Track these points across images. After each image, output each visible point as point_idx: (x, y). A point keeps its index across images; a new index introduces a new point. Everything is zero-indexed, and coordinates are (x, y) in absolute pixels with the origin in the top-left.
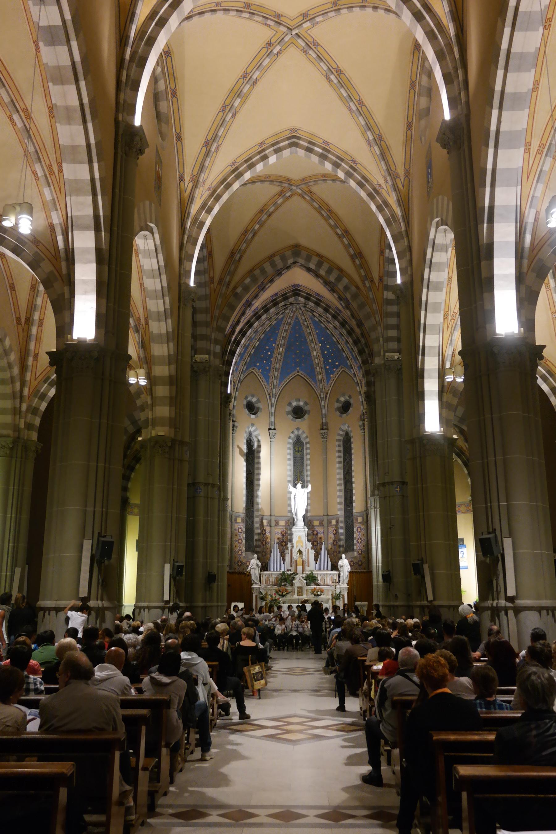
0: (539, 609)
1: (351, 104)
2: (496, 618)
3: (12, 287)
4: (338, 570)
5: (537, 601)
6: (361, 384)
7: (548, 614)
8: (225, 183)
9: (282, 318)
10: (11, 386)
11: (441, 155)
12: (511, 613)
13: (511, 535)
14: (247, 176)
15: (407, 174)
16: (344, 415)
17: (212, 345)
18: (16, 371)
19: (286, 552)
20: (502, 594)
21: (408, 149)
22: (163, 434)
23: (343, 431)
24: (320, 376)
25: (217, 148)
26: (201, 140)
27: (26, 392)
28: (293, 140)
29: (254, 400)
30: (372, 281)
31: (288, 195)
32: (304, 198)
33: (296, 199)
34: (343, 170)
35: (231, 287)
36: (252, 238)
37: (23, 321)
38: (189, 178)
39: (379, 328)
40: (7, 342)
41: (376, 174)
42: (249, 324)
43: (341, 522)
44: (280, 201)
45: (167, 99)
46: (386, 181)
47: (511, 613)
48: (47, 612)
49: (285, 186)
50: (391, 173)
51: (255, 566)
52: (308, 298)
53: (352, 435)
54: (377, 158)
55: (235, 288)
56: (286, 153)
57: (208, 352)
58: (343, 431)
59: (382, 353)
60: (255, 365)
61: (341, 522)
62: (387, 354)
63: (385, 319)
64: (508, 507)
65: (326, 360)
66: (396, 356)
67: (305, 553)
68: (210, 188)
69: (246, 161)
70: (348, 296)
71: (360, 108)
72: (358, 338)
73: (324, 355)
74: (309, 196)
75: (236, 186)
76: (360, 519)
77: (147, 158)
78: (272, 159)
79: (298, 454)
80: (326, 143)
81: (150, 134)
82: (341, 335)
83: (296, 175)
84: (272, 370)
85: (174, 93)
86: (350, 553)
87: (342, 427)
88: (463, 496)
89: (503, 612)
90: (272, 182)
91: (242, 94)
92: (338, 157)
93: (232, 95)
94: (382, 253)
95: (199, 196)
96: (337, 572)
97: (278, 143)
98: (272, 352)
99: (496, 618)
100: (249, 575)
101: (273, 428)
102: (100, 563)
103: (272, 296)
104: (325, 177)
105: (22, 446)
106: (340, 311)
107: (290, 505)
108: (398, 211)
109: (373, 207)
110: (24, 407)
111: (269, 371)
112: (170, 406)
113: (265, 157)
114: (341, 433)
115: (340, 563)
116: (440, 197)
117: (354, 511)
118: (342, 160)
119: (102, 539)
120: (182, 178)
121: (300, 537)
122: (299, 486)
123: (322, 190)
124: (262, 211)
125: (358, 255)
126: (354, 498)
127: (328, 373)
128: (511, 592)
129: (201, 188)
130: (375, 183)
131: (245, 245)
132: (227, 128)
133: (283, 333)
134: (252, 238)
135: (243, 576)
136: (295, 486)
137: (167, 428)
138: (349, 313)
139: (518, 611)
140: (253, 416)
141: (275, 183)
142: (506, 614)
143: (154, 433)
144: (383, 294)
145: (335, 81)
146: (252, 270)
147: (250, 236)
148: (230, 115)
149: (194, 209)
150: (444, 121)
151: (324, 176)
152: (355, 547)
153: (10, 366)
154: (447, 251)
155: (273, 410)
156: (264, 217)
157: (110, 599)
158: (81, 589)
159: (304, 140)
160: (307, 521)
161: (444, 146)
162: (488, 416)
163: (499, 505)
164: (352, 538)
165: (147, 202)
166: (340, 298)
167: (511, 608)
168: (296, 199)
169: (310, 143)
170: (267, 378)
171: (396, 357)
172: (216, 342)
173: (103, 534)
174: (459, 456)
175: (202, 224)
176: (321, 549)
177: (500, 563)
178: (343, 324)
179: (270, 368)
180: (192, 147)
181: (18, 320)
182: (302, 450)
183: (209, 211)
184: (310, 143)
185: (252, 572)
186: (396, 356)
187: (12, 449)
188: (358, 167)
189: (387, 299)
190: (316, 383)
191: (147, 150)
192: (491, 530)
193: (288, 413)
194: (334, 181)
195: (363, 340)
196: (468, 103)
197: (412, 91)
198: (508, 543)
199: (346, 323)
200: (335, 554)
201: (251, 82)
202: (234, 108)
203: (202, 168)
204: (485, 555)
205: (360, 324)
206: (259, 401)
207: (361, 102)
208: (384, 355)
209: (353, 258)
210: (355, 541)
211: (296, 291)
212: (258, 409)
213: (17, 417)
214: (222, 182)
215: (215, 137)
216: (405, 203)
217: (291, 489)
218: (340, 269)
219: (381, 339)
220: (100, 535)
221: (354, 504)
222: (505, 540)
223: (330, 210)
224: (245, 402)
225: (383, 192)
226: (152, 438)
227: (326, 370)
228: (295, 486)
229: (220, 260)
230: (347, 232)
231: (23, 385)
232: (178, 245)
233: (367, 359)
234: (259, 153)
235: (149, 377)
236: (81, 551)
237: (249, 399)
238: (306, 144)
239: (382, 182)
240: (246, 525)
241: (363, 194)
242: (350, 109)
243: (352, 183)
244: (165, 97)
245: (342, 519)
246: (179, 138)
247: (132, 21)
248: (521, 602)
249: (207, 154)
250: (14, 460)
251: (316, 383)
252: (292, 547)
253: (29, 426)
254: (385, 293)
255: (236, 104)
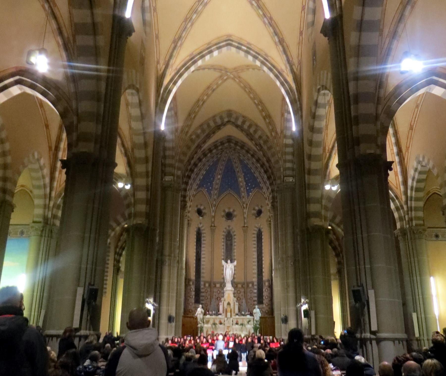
0: (393, 340)
1: (265, 19)
2: (364, 346)
3: (47, 126)
4: (253, 316)
5: (394, 335)
6: (268, 198)
7: (399, 343)
8: (186, 66)
9: (221, 157)
10: (43, 190)
11: (323, 41)
12: (374, 342)
13: (373, 288)
14: (200, 63)
15: (300, 63)
16: (258, 218)
17: (176, 170)
18: (47, 180)
19: (220, 303)
20: (368, 330)
21: (300, 47)
22: (140, 222)
23: (256, 227)
24: (243, 194)
25: (181, 45)
26: (171, 38)
27: (53, 194)
28: (228, 42)
29: (202, 208)
30: (276, 133)
31: (225, 78)
32: (235, 81)
33: (230, 82)
34: (260, 61)
35: (189, 135)
36: (202, 105)
37: (53, 148)
38: (163, 62)
39: (280, 161)
40: (42, 161)
41: (281, 63)
42: (200, 160)
43: (256, 285)
44: (220, 82)
45: (150, 12)
46: (286, 68)
47: (374, 342)
48: (51, 338)
49: (222, 71)
50: (289, 62)
51: (200, 312)
52: (236, 143)
53: (262, 230)
54: (280, 53)
55: (191, 136)
56: (224, 49)
57: (173, 175)
58: (256, 227)
59: (282, 177)
60: (203, 186)
61: (256, 285)
62: (285, 178)
63: (284, 156)
64: (371, 269)
65: (247, 184)
66: (291, 179)
67: (232, 305)
68: (176, 69)
69: (199, 54)
70: (262, 142)
71: (271, 23)
72: (267, 169)
73: (246, 181)
74: (237, 78)
75: (192, 68)
76: (267, 284)
77: (133, 39)
78: (216, 53)
79: (229, 242)
80: (249, 43)
81: (136, 24)
82: (257, 168)
83: (230, 65)
84: (213, 189)
85: (155, 10)
86: (261, 306)
87: (256, 225)
88: (333, 270)
89: (369, 342)
90: (215, 69)
91: (197, 12)
92: (256, 53)
93: (191, 12)
94: (283, 115)
95: (169, 74)
96: (253, 317)
97: (219, 43)
98: (214, 178)
99: (364, 346)
100: (196, 318)
101: (213, 225)
102: (89, 304)
103: (214, 143)
104: (248, 67)
105: (49, 230)
106: (255, 151)
107: (223, 274)
108: (293, 85)
109: (278, 83)
110: (52, 204)
111: (211, 190)
112: (147, 204)
113: (211, 52)
114: (256, 229)
115: (255, 311)
116: (322, 72)
117: (264, 279)
118: (259, 54)
119: (91, 287)
120: (158, 62)
121: (229, 294)
122: (229, 261)
123: (246, 76)
124: (209, 88)
125: (268, 117)
126: (263, 270)
127: (248, 192)
128: (374, 327)
129: (170, 69)
130: (279, 68)
131: (198, 109)
132: (187, 32)
133: (221, 167)
134: (202, 105)
135: (192, 319)
136: (227, 262)
137: (144, 219)
138: (261, 153)
139: (379, 341)
140: (201, 218)
141: (217, 70)
142: (371, 343)
143: (135, 222)
144: (283, 141)
145: (255, 5)
146: (201, 125)
147: (201, 103)
148: (190, 24)
149: (166, 82)
150: (325, 19)
151: (248, 66)
152: (264, 301)
153: (43, 177)
154: (325, 108)
155: (213, 214)
156: (210, 92)
157: (94, 330)
158: (74, 322)
159: (236, 42)
160: (234, 284)
161: (325, 36)
162: (356, 207)
163: (365, 267)
164: (262, 296)
165: (134, 71)
166: (256, 145)
167: (374, 339)
168: (230, 82)
169: (239, 43)
170: (210, 194)
171: (291, 180)
172: (179, 169)
173: (92, 283)
174: (330, 244)
175: (170, 91)
176: (242, 302)
177: (366, 308)
178: (258, 160)
179: (212, 189)
180: (165, 44)
181: (50, 148)
182: (231, 240)
183: (175, 83)
184: (239, 43)
185: (198, 316)
186: (291, 179)
187: (42, 231)
188: (269, 59)
189: (285, 144)
190: (240, 197)
191: (133, 34)
192: (359, 284)
193: (223, 217)
194: (253, 69)
195: (270, 171)
196: (341, 8)
197: (303, 12)
198: (371, 293)
199: (260, 160)
200: (251, 306)
201: (203, 4)
202: (192, 20)
203: (171, 57)
204: (356, 301)
205: (269, 161)
206: (205, 208)
207: (271, 18)
208: (284, 178)
209: (264, 118)
210: (264, 298)
211: (229, 139)
212: (205, 213)
213: (47, 210)
214: (183, 66)
215: (180, 38)
216: (297, 80)
217: (223, 262)
218: (257, 125)
219: (282, 169)
220: (90, 284)
221: (264, 274)
222: (369, 291)
223: (251, 88)
224: (196, 209)
225: (285, 74)
226: (134, 225)
227: (247, 190)
228: (227, 262)
229: (182, 117)
230: (261, 102)
231: (51, 190)
232: (154, 104)
233: (273, 182)
234: (207, 49)
235: (133, 185)
236: (75, 296)
237: (199, 207)
238: (236, 44)
239: (283, 67)
240: (195, 287)
241: (272, 75)
242: (264, 23)
243: (265, 69)
244: (149, 11)
245: (256, 283)
246: (157, 37)
247: (161, 87)
248: (382, 335)
249: (174, 48)
250: (43, 238)
251: (240, 197)
252: (225, 300)
253: (54, 217)
254: (285, 140)
255: (194, 17)
